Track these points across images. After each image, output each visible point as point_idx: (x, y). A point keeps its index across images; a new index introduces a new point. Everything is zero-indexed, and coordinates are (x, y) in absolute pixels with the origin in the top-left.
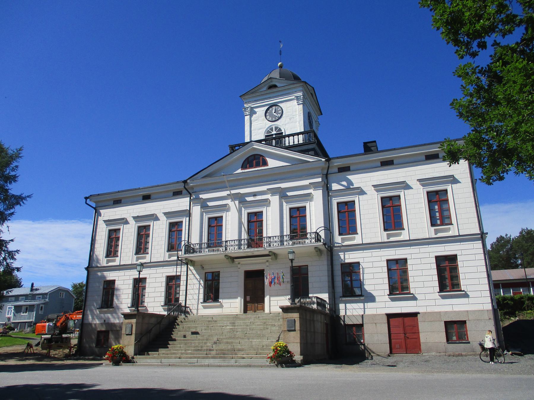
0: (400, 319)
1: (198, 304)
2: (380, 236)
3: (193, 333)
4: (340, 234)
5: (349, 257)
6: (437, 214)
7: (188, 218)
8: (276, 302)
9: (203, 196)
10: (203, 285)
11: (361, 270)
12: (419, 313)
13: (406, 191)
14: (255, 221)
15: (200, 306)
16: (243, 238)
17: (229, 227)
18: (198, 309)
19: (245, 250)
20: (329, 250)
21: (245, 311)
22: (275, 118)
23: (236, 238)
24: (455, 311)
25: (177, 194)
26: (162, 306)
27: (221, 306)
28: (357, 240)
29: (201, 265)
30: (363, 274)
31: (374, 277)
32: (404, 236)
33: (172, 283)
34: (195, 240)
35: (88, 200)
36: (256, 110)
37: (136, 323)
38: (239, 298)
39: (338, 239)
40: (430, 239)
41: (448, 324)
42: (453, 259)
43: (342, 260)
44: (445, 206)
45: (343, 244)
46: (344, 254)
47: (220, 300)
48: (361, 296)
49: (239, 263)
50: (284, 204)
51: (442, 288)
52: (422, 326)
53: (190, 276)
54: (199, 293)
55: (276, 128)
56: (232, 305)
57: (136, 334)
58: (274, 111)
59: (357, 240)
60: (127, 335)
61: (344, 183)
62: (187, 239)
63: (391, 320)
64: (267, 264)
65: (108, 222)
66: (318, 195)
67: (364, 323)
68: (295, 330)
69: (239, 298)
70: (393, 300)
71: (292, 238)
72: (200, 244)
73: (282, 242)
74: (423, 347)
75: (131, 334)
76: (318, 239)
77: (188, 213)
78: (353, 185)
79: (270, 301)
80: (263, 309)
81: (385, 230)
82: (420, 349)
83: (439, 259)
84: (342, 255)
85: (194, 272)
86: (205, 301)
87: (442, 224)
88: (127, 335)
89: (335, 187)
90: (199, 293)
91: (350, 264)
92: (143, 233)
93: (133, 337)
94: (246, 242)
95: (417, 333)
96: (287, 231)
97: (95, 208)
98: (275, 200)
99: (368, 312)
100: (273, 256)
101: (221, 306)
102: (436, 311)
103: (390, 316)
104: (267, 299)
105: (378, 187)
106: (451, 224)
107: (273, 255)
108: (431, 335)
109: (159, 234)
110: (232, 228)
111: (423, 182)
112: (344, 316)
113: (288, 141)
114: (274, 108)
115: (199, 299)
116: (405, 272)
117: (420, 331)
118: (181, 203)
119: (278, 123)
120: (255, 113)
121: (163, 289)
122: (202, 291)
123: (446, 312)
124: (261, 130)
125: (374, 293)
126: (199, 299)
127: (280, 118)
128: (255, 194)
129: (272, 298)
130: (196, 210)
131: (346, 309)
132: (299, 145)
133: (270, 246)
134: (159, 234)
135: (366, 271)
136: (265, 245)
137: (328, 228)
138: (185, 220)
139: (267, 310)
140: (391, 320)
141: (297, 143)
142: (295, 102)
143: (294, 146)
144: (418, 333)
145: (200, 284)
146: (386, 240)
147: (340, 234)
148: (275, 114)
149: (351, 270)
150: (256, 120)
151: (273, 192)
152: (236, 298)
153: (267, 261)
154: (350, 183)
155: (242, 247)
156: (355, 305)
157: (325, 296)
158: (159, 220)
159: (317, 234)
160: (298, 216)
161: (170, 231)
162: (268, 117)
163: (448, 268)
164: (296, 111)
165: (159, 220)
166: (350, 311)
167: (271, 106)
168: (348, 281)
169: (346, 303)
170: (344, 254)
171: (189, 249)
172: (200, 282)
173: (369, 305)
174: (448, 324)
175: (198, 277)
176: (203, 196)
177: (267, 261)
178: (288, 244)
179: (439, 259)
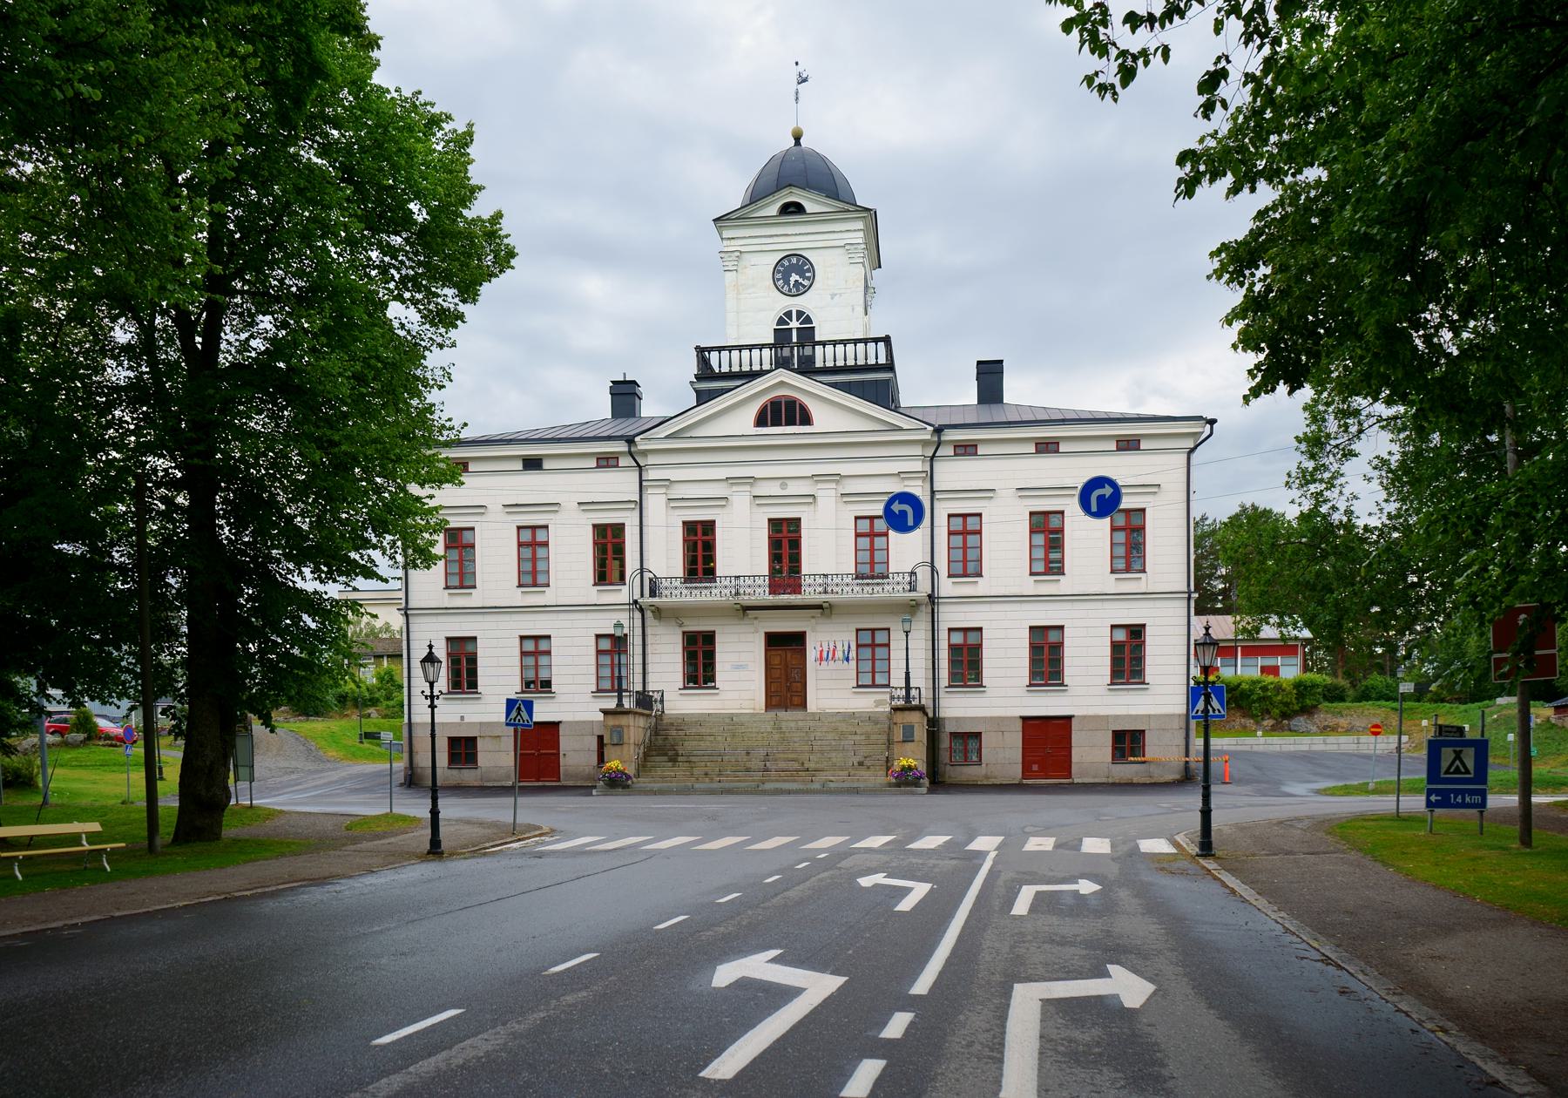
19: (763, 596)
25: (606, 462)
31: (1006, 658)
41: (1118, 736)
55: (800, 314)
102: (1133, 712)
107: (822, 609)
118: (620, 484)
143: (835, 370)
166: (958, 707)
174: (1118, 736)
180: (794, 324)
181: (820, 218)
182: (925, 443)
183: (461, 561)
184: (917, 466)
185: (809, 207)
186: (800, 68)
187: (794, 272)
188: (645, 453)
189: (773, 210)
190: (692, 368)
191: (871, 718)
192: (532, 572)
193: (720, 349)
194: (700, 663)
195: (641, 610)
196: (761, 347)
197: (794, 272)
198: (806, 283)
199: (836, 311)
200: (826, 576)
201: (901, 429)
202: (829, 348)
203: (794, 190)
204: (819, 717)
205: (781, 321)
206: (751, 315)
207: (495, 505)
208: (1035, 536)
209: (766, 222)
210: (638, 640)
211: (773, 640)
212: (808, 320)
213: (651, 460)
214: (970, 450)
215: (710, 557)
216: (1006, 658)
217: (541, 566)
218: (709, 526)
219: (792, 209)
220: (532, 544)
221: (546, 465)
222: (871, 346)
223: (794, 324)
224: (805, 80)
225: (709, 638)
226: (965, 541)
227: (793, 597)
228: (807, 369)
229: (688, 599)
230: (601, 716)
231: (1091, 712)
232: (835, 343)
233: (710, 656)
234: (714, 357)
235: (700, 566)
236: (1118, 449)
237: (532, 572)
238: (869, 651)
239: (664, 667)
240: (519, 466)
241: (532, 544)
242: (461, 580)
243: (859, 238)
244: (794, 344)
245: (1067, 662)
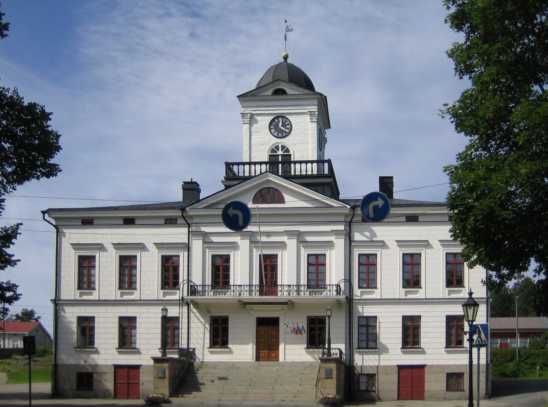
0: (410, 370)
1: (204, 349)
2: (399, 292)
3: (221, 378)
4: (360, 287)
5: (368, 311)
6: (127, 278)
7: (187, 253)
8: (294, 352)
9: (205, 229)
10: (209, 329)
11: (378, 324)
12: (426, 365)
13: (427, 250)
14: (269, 266)
15: (206, 350)
16: (254, 284)
17: (285, 268)
18: (203, 354)
19: (256, 296)
20: (349, 304)
21: (258, 358)
22: (282, 134)
23: (247, 283)
24: (456, 365)
25: (170, 222)
26: (116, 348)
27: (231, 352)
28: (376, 294)
29: (207, 309)
30: (379, 328)
31: (390, 332)
32: (136, 296)
33: (169, 326)
34: (197, 280)
35: (46, 215)
36: (258, 118)
37: (169, 367)
38: (251, 345)
39: (357, 292)
40: (443, 299)
41: (450, 376)
42: (91, 319)
43: (360, 313)
44: (92, 272)
45: (363, 298)
46: (363, 308)
47: (229, 346)
48: (376, 348)
49: (251, 309)
50: (302, 249)
51: (448, 344)
52: (427, 377)
53: (193, 319)
54: (204, 338)
55: (283, 147)
56: (242, 351)
57: (170, 378)
58: (280, 124)
59: (376, 294)
60: (159, 378)
61: (367, 234)
62: (186, 278)
63: (401, 370)
64: (283, 312)
65: (76, 246)
66: (340, 243)
67: (379, 372)
68: (332, 378)
69: (251, 345)
70: (404, 353)
71: (309, 286)
72: (204, 286)
73: (298, 292)
74: (426, 394)
75: (164, 378)
76: (338, 292)
77: (188, 247)
78: (376, 236)
79: (285, 349)
80: (277, 358)
81: (404, 287)
82: (424, 396)
83: (121, 319)
84: (360, 308)
85: (198, 314)
86: (211, 347)
87: (368, 287)
88: (159, 378)
89: (357, 237)
90: (204, 338)
91: (368, 318)
92: (86, 264)
93: (166, 381)
94: (258, 289)
95: (423, 382)
96: (304, 281)
97: (55, 226)
98: (292, 243)
99: (382, 363)
100: (291, 306)
101: (231, 352)
102: (441, 364)
103: (401, 368)
104: (281, 347)
105: (401, 243)
106: (376, 288)
107: (288, 304)
108: (434, 384)
109: (149, 270)
110: (243, 271)
111: (159, 246)
112: (361, 366)
113: (297, 170)
114: (281, 119)
115: (204, 344)
116: (418, 327)
117: (426, 380)
118: (178, 234)
119: (285, 141)
120: (257, 122)
121: (159, 331)
122: (208, 335)
123: (449, 366)
124: (263, 147)
125: (389, 346)
126: (204, 344)
127: (288, 134)
128: (268, 234)
129: (287, 346)
130: (197, 245)
131: (363, 360)
132: (307, 177)
133: (289, 294)
134: (149, 270)
135: (382, 325)
136: (279, 293)
137: (349, 281)
138: (183, 256)
139: (281, 359)
140: (401, 370)
141: (310, 173)
142: (308, 118)
143: (301, 177)
144: (424, 383)
145: (205, 328)
146: (404, 297)
147: (360, 287)
148: (282, 128)
149: (369, 325)
150: (257, 132)
151: (290, 234)
152: (249, 344)
153: (283, 309)
154: (373, 234)
155: (254, 293)
156: (371, 357)
157: (342, 347)
158: (148, 250)
159: (338, 286)
160: (317, 264)
161: (121, 266)
162: (273, 131)
163: (411, 327)
164: (308, 130)
165: (148, 250)
166: (364, 361)
167: (278, 117)
168: (366, 334)
169: (362, 353)
170: (363, 308)
171: (193, 290)
172: (205, 325)
173: (383, 356)
174: (450, 376)
175: (203, 321)
176: (205, 229)
177: (283, 309)
178: (305, 294)
179: (121, 319)
180: (280, 152)
181: (295, 98)
182: (346, 215)
183: (368, 273)
184: (342, 227)
185: (289, 91)
186: (288, 24)
187: (280, 127)
188: (192, 217)
189: (270, 92)
190: (222, 173)
191: (311, 365)
192: (412, 280)
193: (238, 164)
194: (220, 336)
195: (188, 305)
196: (312, 162)
197: (280, 127)
198: (287, 131)
199: (302, 144)
200: (289, 286)
201: (333, 207)
202: (298, 165)
203: (281, 83)
204: (283, 365)
205: (273, 151)
206: (259, 144)
207: (391, 243)
208: (310, 267)
209: (265, 99)
210: (185, 320)
211: (261, 322)
212: (288, 150)
213: (195, 220)
214: (173, 221)
215: (227, 277)
216: (390, 332)
217: (371, 276)
218: (227, 259)
219: (280, 92)
220: (127, 267)
221: (137, 222)
222: (253, 166)
223: (280, 152)
224: (291, 30)
225: (225, 320)
226: (412, 269)
227: (271, 297)
228: (287, 176)
229: (212, 297)
230: (152, 362)
231: (435, 363)
232: (301, 162)
233: (225, 330)
234: (235, 168)
235: (221, 279)
236: (166, 223)
237: (412, 280)
238: (364, 329)
239: (196, 334)
240: (404, 219)
241: (127, 267)
242: (368, 284)
243: (315, 109)
244: (280, 162)
245: (422, 335)
